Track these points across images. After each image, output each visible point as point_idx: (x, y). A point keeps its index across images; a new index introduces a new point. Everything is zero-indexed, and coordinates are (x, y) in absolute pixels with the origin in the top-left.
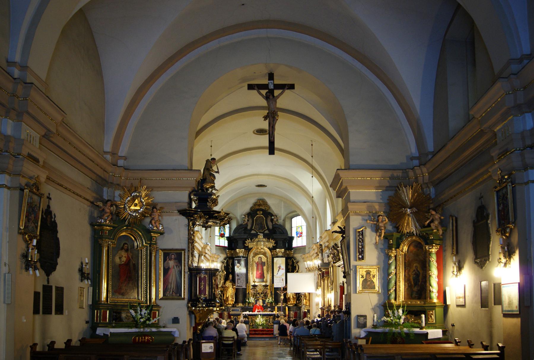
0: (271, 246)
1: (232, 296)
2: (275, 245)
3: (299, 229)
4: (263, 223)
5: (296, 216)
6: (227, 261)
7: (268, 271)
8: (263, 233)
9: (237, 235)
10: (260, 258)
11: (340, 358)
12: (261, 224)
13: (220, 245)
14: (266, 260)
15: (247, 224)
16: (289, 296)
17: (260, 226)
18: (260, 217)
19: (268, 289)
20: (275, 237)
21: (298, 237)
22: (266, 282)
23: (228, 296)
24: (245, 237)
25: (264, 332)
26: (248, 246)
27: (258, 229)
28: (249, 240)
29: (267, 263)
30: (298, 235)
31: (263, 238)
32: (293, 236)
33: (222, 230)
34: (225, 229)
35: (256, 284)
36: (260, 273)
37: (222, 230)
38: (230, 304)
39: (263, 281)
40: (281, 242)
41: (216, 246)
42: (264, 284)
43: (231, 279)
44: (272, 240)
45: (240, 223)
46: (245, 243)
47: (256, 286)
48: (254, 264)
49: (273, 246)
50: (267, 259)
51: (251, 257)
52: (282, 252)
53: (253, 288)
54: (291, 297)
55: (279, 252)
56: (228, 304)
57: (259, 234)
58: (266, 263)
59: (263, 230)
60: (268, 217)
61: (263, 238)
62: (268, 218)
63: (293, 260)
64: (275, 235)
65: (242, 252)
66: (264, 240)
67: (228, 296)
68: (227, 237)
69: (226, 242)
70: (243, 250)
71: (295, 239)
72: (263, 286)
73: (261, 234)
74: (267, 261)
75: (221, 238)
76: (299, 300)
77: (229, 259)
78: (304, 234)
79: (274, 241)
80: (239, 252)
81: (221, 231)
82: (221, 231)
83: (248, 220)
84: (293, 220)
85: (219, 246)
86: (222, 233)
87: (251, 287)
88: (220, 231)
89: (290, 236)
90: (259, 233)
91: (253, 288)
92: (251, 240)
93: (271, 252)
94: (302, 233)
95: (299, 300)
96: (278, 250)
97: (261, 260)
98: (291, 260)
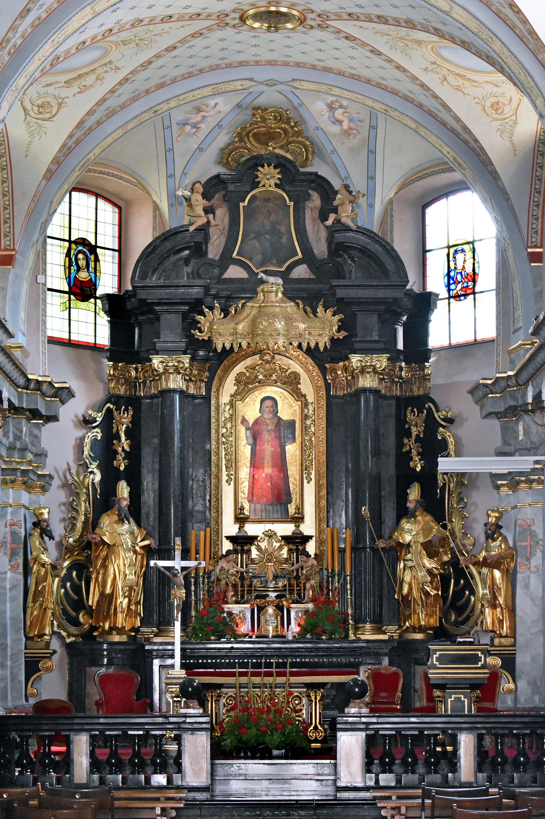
0: (324, 341)
1: (131, 588)
2: (342, 335)
3: (460, 256)
4: (283, 229)
5: (446, 195)
6: (109, 416)
7: (304, 468)
8: (285, 275)
9: (154, 280)
10: (269, 403)
11: (359, 620)
12: (274, 232)
13: (74, 337)
14: (298, 411)
15: (204, 229)
16: (405, 591)
17: (267, 244)
18: (268, 198)
19: (309, 556)
20: (341, 293)
21: (457, 297)
22: (298, 519)
23: (108, 591)
24: (196, 292)
25: (301, 284)
26: (209, 342)
27: (258, 258)
28: (211, 308)
29: (305, 429)
30: (457, 289)
31: (282, 301)
32: (429, 289)
33: (82, 263)
34: (97, 260)
35: (251, 529)
36: (270, 477)
37: (82, 263)
38: (120, 631)
39: (285, 518)
40: (374, 319)
41: (52, 341)
42: (287, 529)
43: (125, 504)
44: (329, 312)
45: (170, 224)
46: (195, 324)
47: (252, 539)
48: (242, 430)
49: (332, 340)
50: (305, 405)
51: (225, 398)
52: (375, 371)
53: (235, 551)
54: (415, 593)
55: (363, 371)
56: (111, 629)
57: (262, 282)
58: (298, 425)
59: (280, 265)
60: (308, 197)
61: (282, 301)
62: (309, 204)
63: (429, 410)
64: (342, 282)
65: (177, 371)
66: (290, 306)
67: (108, 591)
68: (108, 297)
69: (104, 320)
70: (186, 359)
71: (441, 306)
72: (284, 538)
73: (271, 279)
74: (304, 417)
75: (74, 302)
76: (460, 610)
77: (118, 409)
78: (542, 192)
79: (337, 317)
80: (166, 371)
81: (79, 269)
82: (79, 269)
83: (208, 210)
84: (429, 211)
85: (69, 344)
86: (83, 275)
87: (227, 546)
88: (74, 268)
89: (417, 289)
90: (261, 275)
91: (235, 551)
92: (225, 311)
93: (324, 371)
94: (474, 277)
95: (460, 610)
96: (355, 360)
97: (275, 412)
98: (420, 411)
